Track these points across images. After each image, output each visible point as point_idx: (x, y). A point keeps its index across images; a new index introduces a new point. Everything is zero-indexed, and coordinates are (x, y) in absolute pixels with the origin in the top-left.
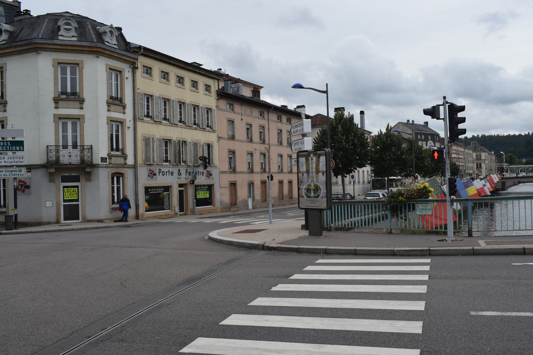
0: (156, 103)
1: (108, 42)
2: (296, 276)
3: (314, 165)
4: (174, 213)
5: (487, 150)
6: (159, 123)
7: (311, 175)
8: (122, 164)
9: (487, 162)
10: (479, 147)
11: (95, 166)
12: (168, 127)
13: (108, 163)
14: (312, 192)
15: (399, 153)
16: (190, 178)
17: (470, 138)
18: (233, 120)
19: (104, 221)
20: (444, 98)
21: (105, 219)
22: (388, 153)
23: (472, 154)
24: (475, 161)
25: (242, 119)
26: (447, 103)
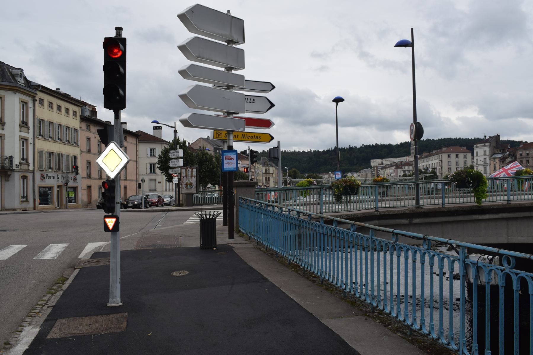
0: (46, 125)
1: (19, 82)
2: (189, 219)
3: (190, 173)
4: (54, 207)
5: (274, 164)
6: (47, 140)
7: (188, 177)
8: (26, 170)
9: (274, 176)
10: (268, 162)
11: (13, 170)
12: (52, 143)
13: (19, 169)
14: (189, 186)
15: (211, 166)
16: (64, 181)
17: (260, 153)
18: (90, 138)
19: (17, 210)
20: (249, 147)
21: (18, 209)
22: (204, 167)
23: (262, 168)
24: (264, 175)
25: (95, 137)
26: (250, 149)
